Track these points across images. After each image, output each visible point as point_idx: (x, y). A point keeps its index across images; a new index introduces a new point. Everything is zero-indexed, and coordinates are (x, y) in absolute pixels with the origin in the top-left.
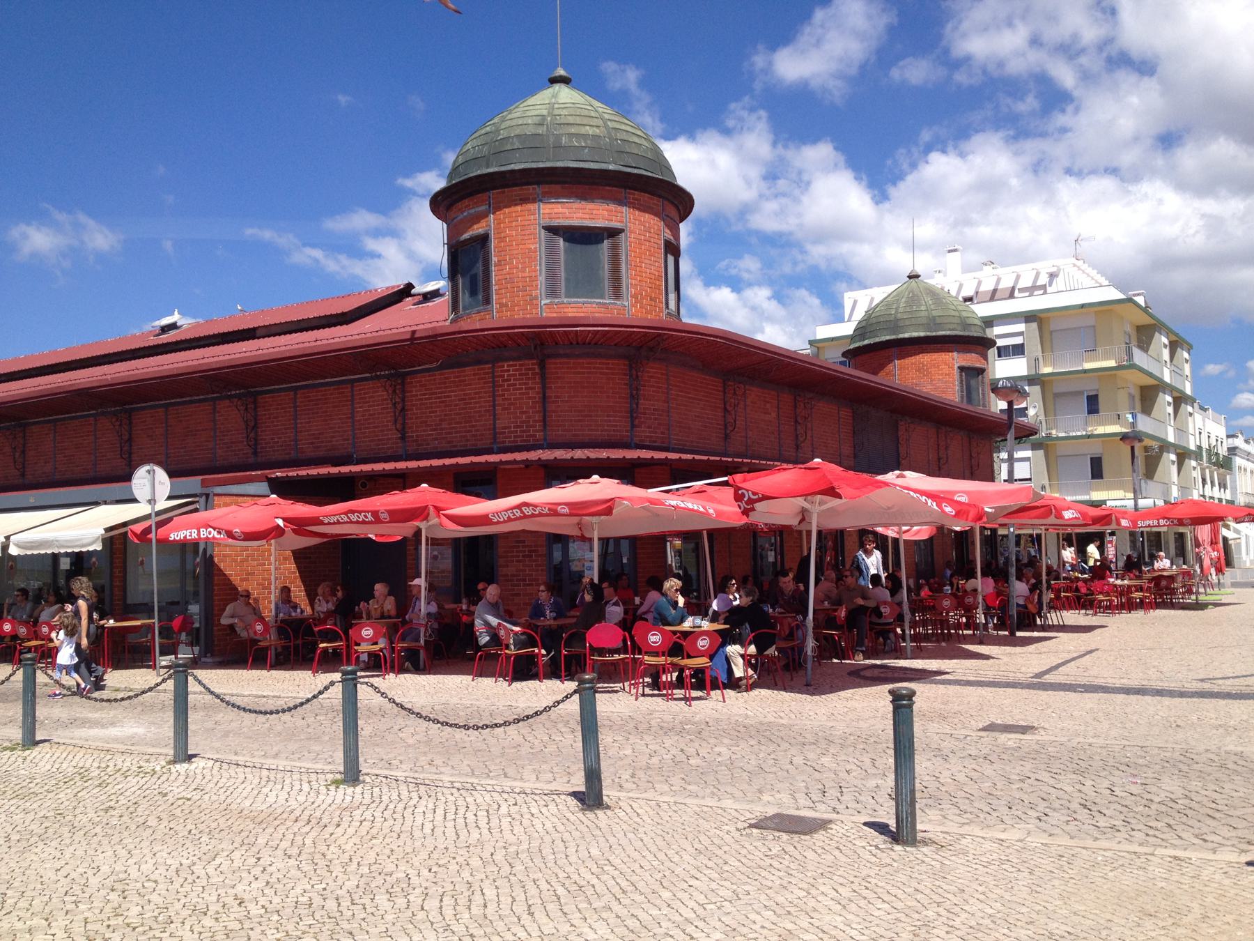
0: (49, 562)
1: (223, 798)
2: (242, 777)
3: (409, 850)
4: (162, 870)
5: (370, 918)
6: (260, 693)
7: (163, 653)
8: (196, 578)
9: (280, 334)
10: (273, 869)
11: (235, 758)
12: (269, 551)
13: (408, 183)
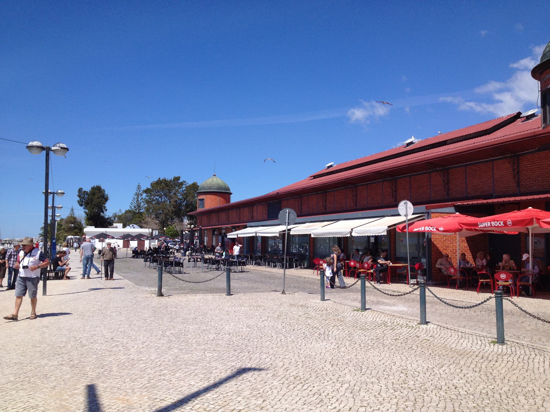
0: (366, 239)
1: (443, 342)
2: (450, 334)
3: (533, 378)
4: (420, 368)
5: (516, 405)
6: (454, 299)
7: (411, 278)
8: (424, 248)
9: (457, 142)
10: (468, 375)
11: (446, 325)
12: (455, 237)
13: (515, 65)
